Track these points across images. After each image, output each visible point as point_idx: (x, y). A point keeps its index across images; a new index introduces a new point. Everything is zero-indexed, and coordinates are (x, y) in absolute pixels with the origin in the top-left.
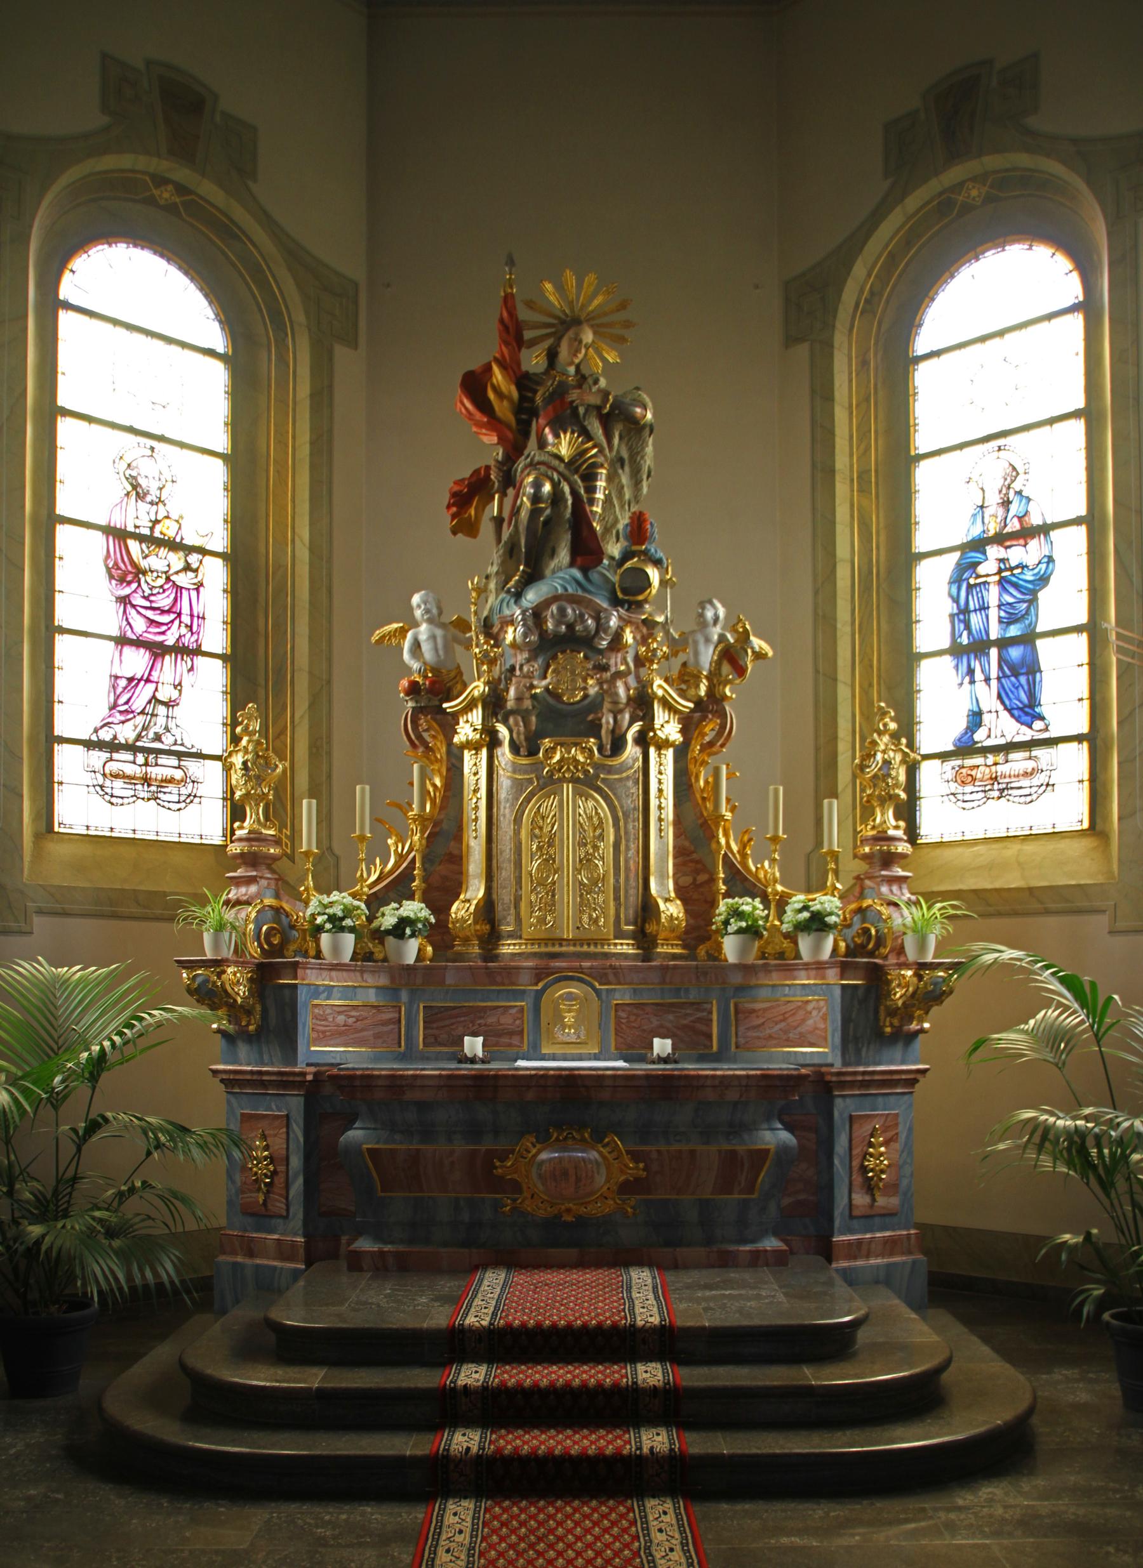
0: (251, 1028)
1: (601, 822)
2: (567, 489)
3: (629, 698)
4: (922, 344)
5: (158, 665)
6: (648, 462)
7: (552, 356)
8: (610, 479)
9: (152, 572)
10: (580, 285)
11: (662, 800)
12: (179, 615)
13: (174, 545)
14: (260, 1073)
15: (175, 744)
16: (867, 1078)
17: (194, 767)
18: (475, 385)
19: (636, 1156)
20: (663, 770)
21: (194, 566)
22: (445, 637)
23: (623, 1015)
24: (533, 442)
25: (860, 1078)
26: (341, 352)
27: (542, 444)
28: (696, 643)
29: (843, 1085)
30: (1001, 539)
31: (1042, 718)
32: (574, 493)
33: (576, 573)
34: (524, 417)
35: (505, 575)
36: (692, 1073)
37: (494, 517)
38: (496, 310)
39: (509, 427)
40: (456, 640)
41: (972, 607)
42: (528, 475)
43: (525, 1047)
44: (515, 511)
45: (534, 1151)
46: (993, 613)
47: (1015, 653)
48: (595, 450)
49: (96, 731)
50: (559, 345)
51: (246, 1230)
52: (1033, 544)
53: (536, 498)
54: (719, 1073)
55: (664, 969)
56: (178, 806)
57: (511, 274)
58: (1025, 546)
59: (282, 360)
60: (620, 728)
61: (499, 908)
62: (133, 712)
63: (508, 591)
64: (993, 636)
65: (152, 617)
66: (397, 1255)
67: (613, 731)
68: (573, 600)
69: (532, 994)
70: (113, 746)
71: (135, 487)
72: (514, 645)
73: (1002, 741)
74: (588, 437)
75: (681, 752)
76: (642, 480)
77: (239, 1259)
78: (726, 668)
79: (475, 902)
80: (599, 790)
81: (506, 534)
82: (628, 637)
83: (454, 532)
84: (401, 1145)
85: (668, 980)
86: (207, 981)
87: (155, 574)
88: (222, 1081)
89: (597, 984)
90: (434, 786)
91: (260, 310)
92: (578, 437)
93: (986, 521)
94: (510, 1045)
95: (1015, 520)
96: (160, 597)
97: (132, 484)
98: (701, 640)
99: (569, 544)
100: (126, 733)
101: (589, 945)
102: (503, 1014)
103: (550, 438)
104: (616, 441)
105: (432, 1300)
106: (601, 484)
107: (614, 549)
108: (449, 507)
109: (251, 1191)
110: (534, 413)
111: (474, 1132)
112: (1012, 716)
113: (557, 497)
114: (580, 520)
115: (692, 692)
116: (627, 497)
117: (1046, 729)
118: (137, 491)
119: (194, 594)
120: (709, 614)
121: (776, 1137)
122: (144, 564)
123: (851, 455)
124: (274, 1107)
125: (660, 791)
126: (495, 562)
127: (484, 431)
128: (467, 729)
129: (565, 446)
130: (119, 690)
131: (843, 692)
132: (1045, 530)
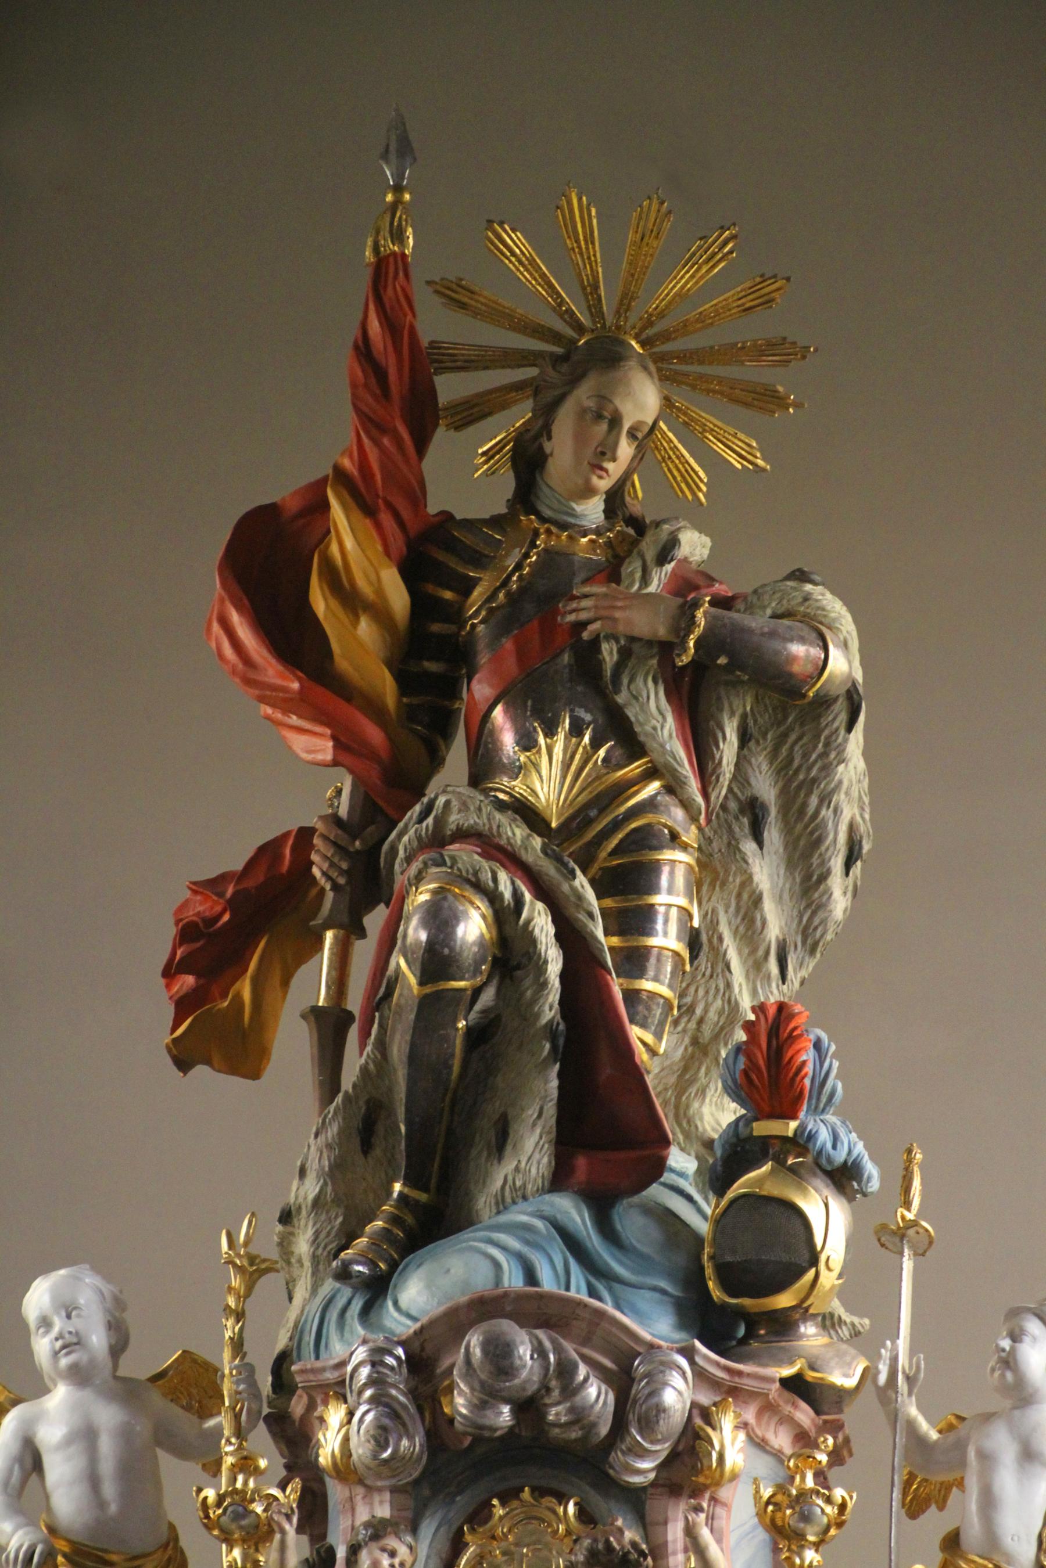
2: (542, 923)
6: (849, 812)
7: (528, 460)
22: (126, 1435)
24: (457, 756)
27: (484, 767)
28: (987, 1459)
32: (570, 935)
33: (571, 1210)
34: (432, 666)
35: (346, 1208)
37: (315, 1010)
38: (346, 310)
39: (374, 709)
42: (419, 878)
48: (654, 786)
50: (546, 431)
53: (437, 961)
57: (398, 189)
63: (344, 1275)
76: (824, 877)
81: (354, 1061)
82: (730, 1442)
83: (183, 1059)
92: (596, 745)
99: (551, 1110)
104: (728, 750)
106: (671, 897)
108: (170, 972)
113: (510, 952)
114: (590, 1037)
126: (313, 1167)
127: (294, 720)
129: (549, 774)
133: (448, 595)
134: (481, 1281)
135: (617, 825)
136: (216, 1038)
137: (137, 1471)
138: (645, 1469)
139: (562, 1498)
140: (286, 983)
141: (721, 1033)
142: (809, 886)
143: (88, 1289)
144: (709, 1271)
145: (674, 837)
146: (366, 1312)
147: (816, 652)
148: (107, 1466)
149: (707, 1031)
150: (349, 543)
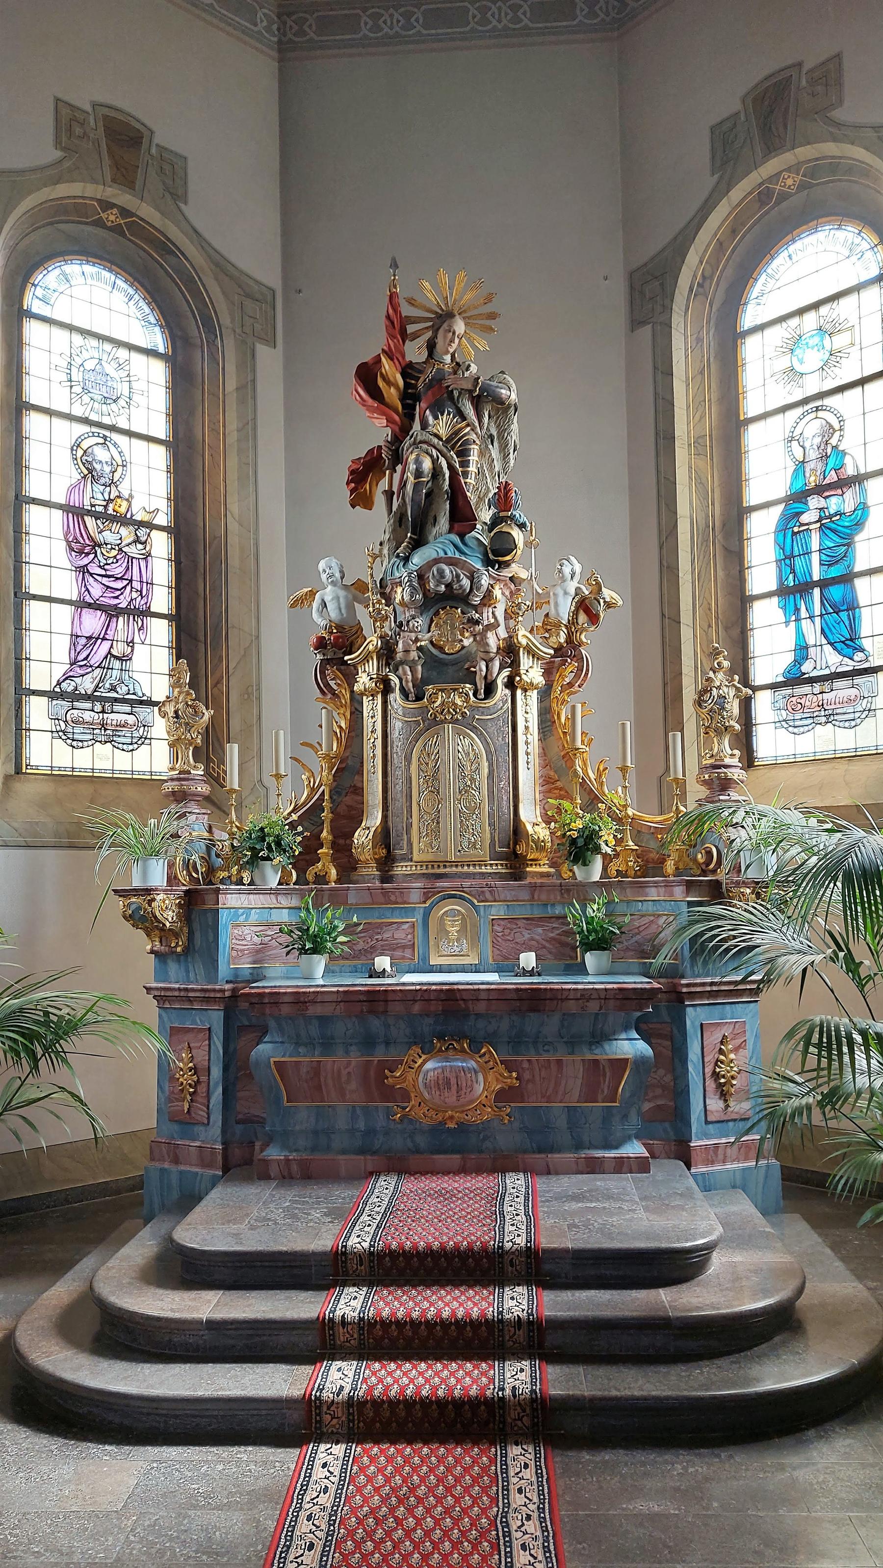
0: (179, 949)
1: (476, 756)
3: (499, 648)
4: (750, 317)
5: (113, 625)
7: (431, 346)
8: (481, 454)
9: (106, 544)
10: (452, 281)
11: (529, 736)
12: (131, 581)
13: (124, 520)
14: (186, 990)
15: (128, 694)
16: (715, 988)
17: (143, 712)
18: (367, 376)
19: (509, 1066)
20: (528, 709)
21: (143, 539)
22: (346, 597)
23: (499, 929)
24: (417, 426)
25: (708, 989)
26: (262, 350)
27: (424, 426)
29: (692, 995)
30: (820, 490)
31: (863, 650)
32: (451, 467)
34: (409, 401)
36: (556, 987)
39: (396, 411)
40: (356, 599)
41: (796, 553)
43: (416, 960)
44: (403, 485)
45: (420, 1061)
46: (815, 558)
47: (836, 592)
48: (468, 429)
49: (59, 684)
51: (173, 1138)
52: (849, 494)
53: (418, 474)
54: (580, 987)
55: (533, 887)
56: (131, 747)
57: (394, 275)
58: (842, 495)
59: (214, 359)
60: (491, 675)
61: (393, 834)
62: (91, 666)
63: (398, 556)
64: (816, 578)
65: (107, 584)
66: (302, 1163)
67: (486, 677)
68: (451, 562)
69: (422, 911)
70: (75, 697)
71: (90, 471)
72: (402, 603)
73: (827, 672)
74: (463, 418)
75: (545, 693)
77: (166, 1165)
78: (582, 618)
79: (374, 829)
80: (474, 729)
82: (497, 592)
84: (305, 1058)
85: (536, 897)
86: (139, 908)
87: (109, 547)
88: (155, 997)
89: (475, 901)
90: (340, 727)
91: (195, 317)
92: (454, 418)
93: (807, 475)
94: (403, 958)
95: (833, 472)
96: (114, 566)
97: (87, 469)
98: (560, 592)
100: (87, 685)
101: (469, 866)
102: (397, 929)
103: (431, 420)
104: (486, 419)
105: (326, 1215)
106: (474, 457)
107: (485, 515)
108: (348, 484)
109: (177, 1100)
110: (417, 398)
111: (368, 1043)
112: (835, 649)
113: (436, 472)
114: (457, 493)
115: (553, 639)
116: (497, 469)
117: (867, 660)
118: (90, 474)
119: (143, 563)
120: (567, 570)
121: (631, 1046)
122: (99, 538)
123: (688, 424)
124: (198, 1021)
125: (527, 728)
128: (363, 681)
130: (79, 648)
131: (686, 633)
132: (859, 479)
133: (413, 382)
134: (434, 555)
135: (459, 439)
136: (361, 499)
137: (351, 608)
138: (476, 600)
139: (457, 608)
140: (377, 485)
141: (486, 494)
142: (505, 457)
143: (334, 563)
144: (489, 551)
145: (474, 442)
146: (404, 565)
147: (508, 393)
148: (343, 606)
149: (482, 495)
150: (387, 367)
